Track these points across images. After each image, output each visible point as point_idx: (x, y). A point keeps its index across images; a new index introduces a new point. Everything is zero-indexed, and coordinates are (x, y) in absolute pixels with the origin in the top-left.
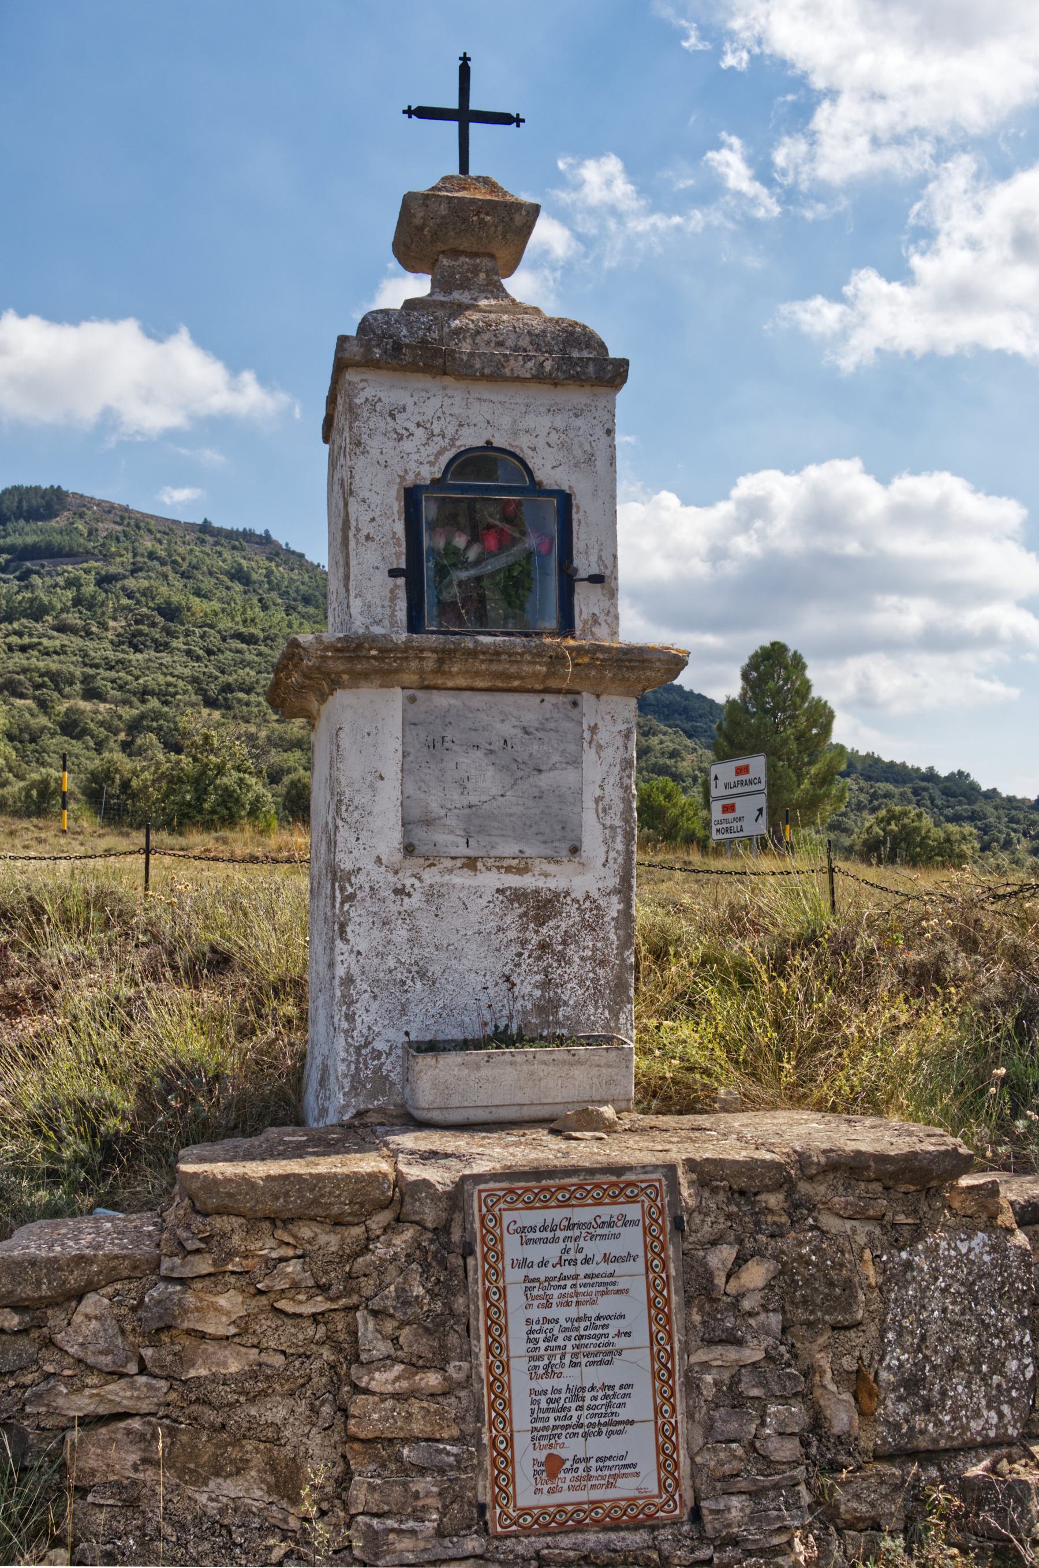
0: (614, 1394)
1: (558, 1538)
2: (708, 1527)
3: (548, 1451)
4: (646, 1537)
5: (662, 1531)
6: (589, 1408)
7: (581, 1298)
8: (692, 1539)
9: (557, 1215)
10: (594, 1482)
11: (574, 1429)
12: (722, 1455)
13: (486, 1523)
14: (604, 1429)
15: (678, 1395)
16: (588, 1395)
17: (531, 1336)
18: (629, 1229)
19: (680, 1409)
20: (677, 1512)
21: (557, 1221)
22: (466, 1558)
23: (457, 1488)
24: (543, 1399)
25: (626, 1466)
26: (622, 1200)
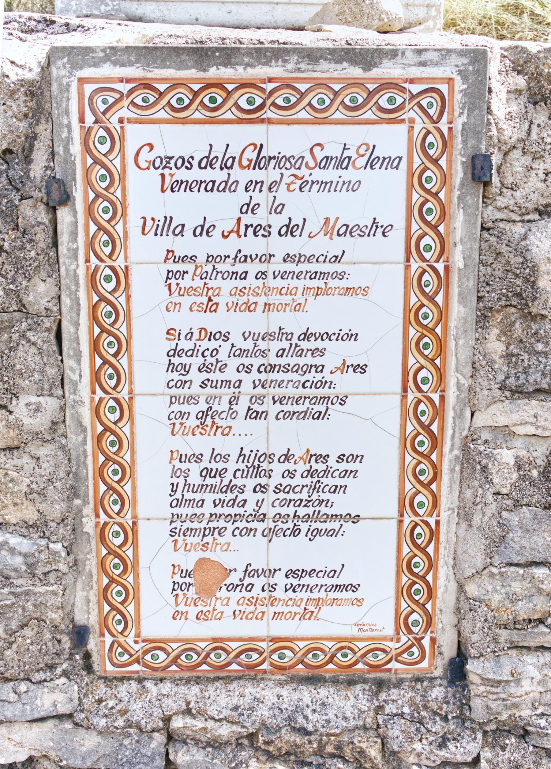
0: (324, 472)
1: (211, 690)
2: (477, 703)
3: (201, 555)
4: (364, 705)
5: (394, 693)
6: (278, 489)
7: (275, 299)
8: (445, 719)
9: (236, 138)
10: (279, 609)
11: (248, 523)
12: (516, 587)
13: (87, 656)
14: (304, 527)
15: (445, 477)
16: (278, 468)
17: (176, 360)
18: (379, 174)
19: (444, 502)
20: (425, 664)
21: (234, 151)
22: (42, 719)
23: (29, 606)
24: (195, 469)
25: (338, 588)
26: (369, 115)
